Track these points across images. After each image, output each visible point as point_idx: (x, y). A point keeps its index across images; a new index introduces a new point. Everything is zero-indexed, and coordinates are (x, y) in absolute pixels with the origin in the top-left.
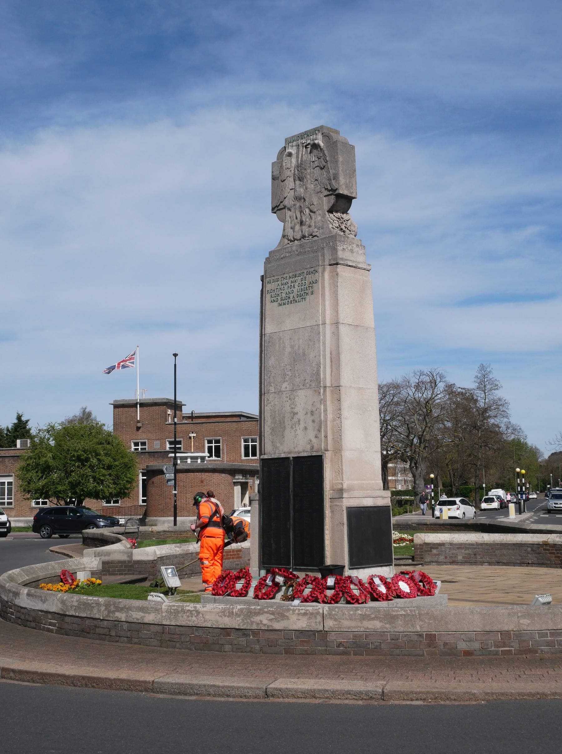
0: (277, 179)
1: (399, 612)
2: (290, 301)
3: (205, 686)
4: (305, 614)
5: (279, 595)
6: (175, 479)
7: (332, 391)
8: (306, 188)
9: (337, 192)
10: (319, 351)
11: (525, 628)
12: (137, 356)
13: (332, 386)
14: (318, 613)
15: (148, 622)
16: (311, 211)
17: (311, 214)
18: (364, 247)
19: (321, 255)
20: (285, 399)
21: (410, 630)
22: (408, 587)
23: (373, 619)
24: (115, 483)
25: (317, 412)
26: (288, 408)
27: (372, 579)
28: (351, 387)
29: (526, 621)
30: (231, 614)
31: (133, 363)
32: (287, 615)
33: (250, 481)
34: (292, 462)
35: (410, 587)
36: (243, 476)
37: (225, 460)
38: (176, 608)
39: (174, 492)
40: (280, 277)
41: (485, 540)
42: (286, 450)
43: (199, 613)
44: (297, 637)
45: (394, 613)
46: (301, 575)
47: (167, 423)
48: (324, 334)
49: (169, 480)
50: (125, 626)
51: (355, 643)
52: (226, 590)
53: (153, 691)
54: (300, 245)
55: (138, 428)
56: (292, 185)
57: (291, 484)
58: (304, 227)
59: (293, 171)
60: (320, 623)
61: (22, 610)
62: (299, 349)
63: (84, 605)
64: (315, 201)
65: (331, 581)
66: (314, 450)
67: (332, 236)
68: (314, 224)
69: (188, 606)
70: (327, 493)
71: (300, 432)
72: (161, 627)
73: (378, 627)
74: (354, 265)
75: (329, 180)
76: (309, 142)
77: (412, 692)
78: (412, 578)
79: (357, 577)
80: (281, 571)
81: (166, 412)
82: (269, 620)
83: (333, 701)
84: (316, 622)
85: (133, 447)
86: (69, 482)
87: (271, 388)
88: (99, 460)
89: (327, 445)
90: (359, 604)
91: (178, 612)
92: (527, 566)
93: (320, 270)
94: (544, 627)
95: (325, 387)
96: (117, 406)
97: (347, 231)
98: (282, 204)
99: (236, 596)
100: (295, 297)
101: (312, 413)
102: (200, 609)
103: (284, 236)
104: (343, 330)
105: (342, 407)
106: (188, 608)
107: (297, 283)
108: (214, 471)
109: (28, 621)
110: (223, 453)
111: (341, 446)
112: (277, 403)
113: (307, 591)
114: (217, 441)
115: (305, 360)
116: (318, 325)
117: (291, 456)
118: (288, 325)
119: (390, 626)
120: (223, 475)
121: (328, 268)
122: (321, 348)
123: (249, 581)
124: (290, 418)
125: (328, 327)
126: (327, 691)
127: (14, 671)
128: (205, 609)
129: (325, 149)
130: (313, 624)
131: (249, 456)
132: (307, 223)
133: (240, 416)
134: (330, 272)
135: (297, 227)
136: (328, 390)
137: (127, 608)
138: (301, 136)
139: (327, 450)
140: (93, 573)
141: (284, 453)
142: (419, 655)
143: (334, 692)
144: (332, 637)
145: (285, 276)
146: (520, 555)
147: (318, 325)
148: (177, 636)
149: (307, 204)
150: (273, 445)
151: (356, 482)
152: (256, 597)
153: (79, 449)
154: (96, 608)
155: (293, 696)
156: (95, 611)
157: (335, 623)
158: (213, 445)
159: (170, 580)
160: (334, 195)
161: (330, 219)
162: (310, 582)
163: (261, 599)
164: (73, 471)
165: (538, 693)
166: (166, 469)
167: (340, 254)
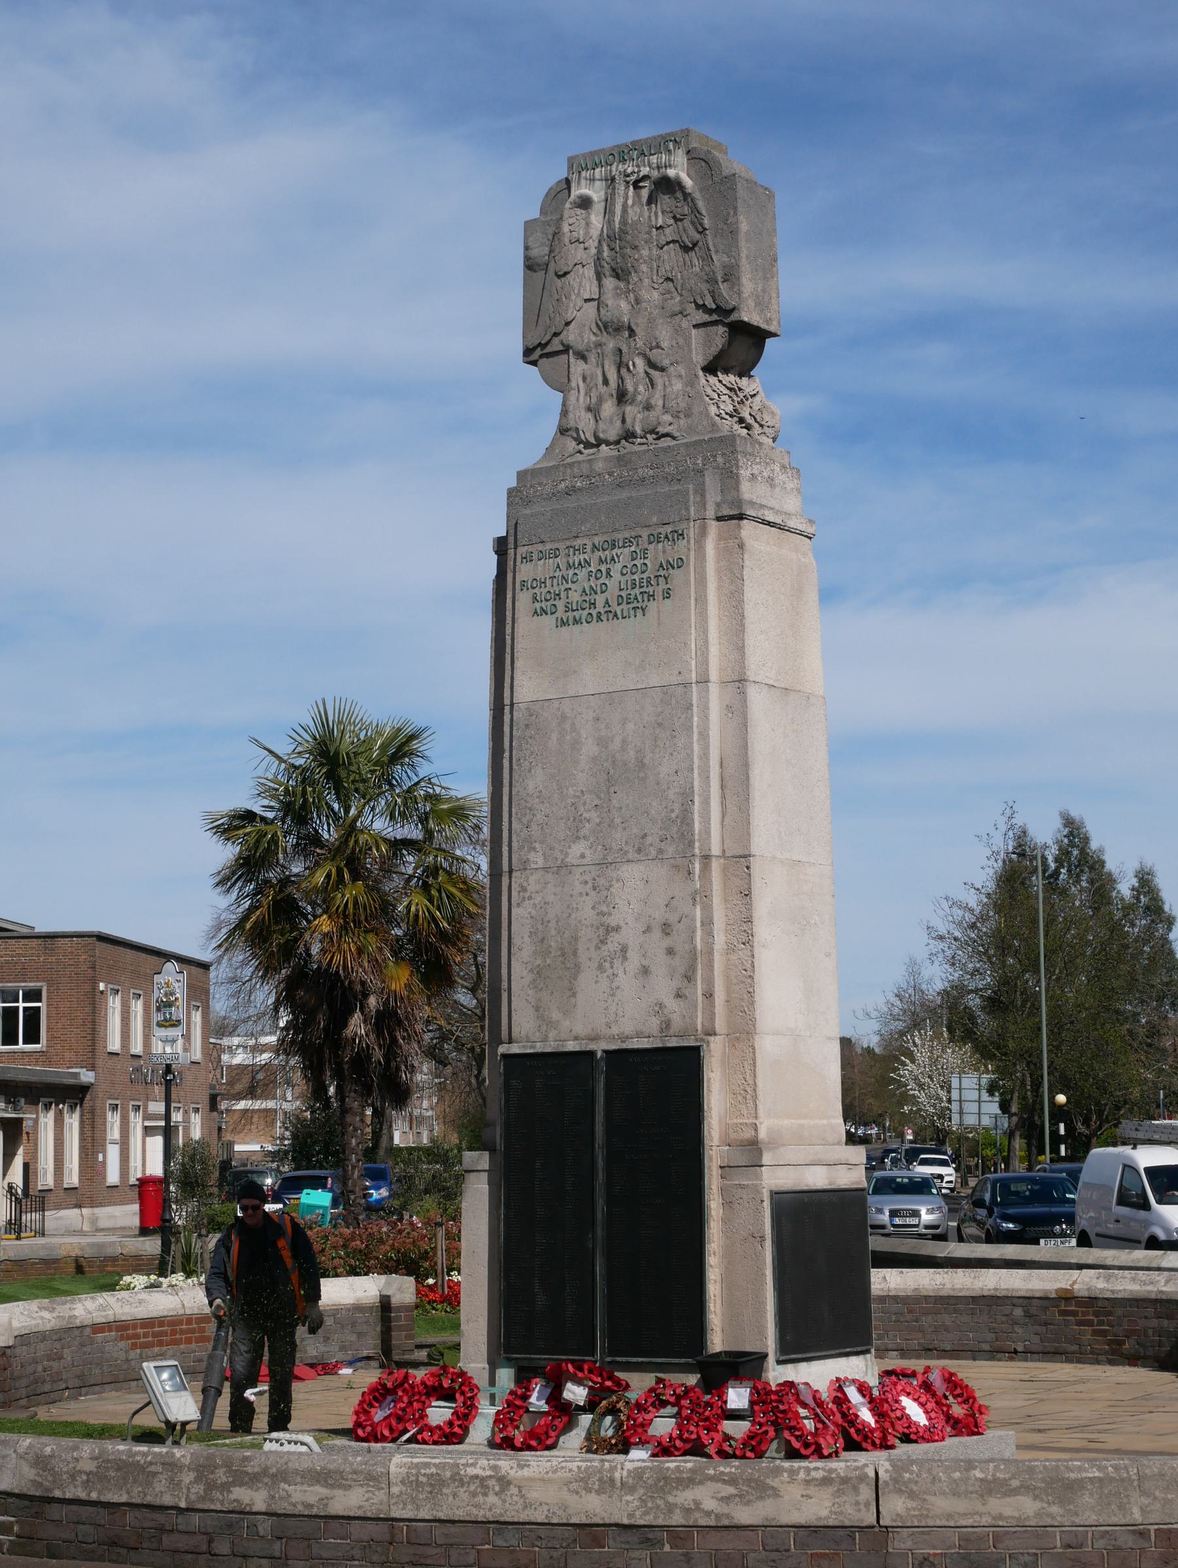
1: (1086, 1471)
2: (594, 613)
4: (826, 1481)
5: (574, 1440)
7: (725, 870)
8: (638, 301)
10: (690, 756)
13: (724, 854)
14: (863, 1478)
15: (341, 1513)
16: (651, 364)
17: (655, 374)
18: (798, 471)
19: (696, 492)
20: (579, 888)
21: (1114, 1520)
22: (920, 1411)
23: (1014, 1492)
25: (681, 926)
26: (587, 914)
27: (840, 1389)
28: (774, 858)
30: (607, 1485)
32: (774, 1484)
33: (28, 1116)
34: (603, 1064)
35: (926, 1412)
36: (8, 1102)
38: (433, 1470)
40: (562, 546)
41: (892, 1286)
42: (580, 1029)
43: (509, 1483)
45: (1073, 1476)
46: (639, 1384)
48: (705, 709)
50: (265, 1526)
51: (965, 1557)
52: (401, 1427)
54: (619, 459)
56: (589, 288)
57: (599, 1129)
58: (628, 409)
59: (593, 251)
60: (867, 1505)
62: (624, 749)
63: (119, 1469)
64: (665, 336)
65: (739, 1395)
66: (671, 1032)
67: (722, 439)
68: (660, 403)
69: (474, 1465)
70: (713, 1153)
71: (627, 980)
72: (385, 1527)
73: (1030, 1513)
74: (779, 521)
75: (712, 281)
76: (645, 171)
78: (927, 1386)
79: (807, 1384)
80: (581, 1369)
82: (722, 1499)
84: (857, 1503)
87: (532, 856)
90: (822, 1457)
91: (443, 1483)
92: (1011, 1359)
93: (692, 531)
97: (757, 429)
98: (556, 340)
99: (435, 1443)
100: (613, 603)
101: (666, 929)
102: (512, 1472)
103: (563, 431)
104: (757, 698)
105: (756, 915)
106: (471, 1471)
107: (618, 566)
111: (753, 1020)
112: (551, 898)
113: (663, 1425)
115: (643, 779)
116: (686, 685)
117: (599, 1047)
118: (589, 680)
119: (1061, 1511)
121: (713, 527)
122: (696, 747)
123: (473, 1398)
124: (595, 941)
125: (714, 690)
128: (526, 1472)
130: (849, 1509)
131: (17, 1043)
132: (639, 398)
134: (720, 538)
135: (609, 408)
136: (715, 865)
137: (274, 1476)
138: (622, 154)
139: (714, 1033)
141: (576, 1038)
144: (901, 1543)
145: (578, 543)
146: (991, 1330)
147: (686, 685)
148: (435, 1551)
149: (640, 344)
150: (541, 1017)
151: (786, 1122)
152: (502, 1443)
154: (162, 1477)
156: (160, 1484)
159: (170, 1401)
160: (725, 325)
161: (709, 391)
162: (672, 1399)
163: (521, 1450)
167: (747, 491)
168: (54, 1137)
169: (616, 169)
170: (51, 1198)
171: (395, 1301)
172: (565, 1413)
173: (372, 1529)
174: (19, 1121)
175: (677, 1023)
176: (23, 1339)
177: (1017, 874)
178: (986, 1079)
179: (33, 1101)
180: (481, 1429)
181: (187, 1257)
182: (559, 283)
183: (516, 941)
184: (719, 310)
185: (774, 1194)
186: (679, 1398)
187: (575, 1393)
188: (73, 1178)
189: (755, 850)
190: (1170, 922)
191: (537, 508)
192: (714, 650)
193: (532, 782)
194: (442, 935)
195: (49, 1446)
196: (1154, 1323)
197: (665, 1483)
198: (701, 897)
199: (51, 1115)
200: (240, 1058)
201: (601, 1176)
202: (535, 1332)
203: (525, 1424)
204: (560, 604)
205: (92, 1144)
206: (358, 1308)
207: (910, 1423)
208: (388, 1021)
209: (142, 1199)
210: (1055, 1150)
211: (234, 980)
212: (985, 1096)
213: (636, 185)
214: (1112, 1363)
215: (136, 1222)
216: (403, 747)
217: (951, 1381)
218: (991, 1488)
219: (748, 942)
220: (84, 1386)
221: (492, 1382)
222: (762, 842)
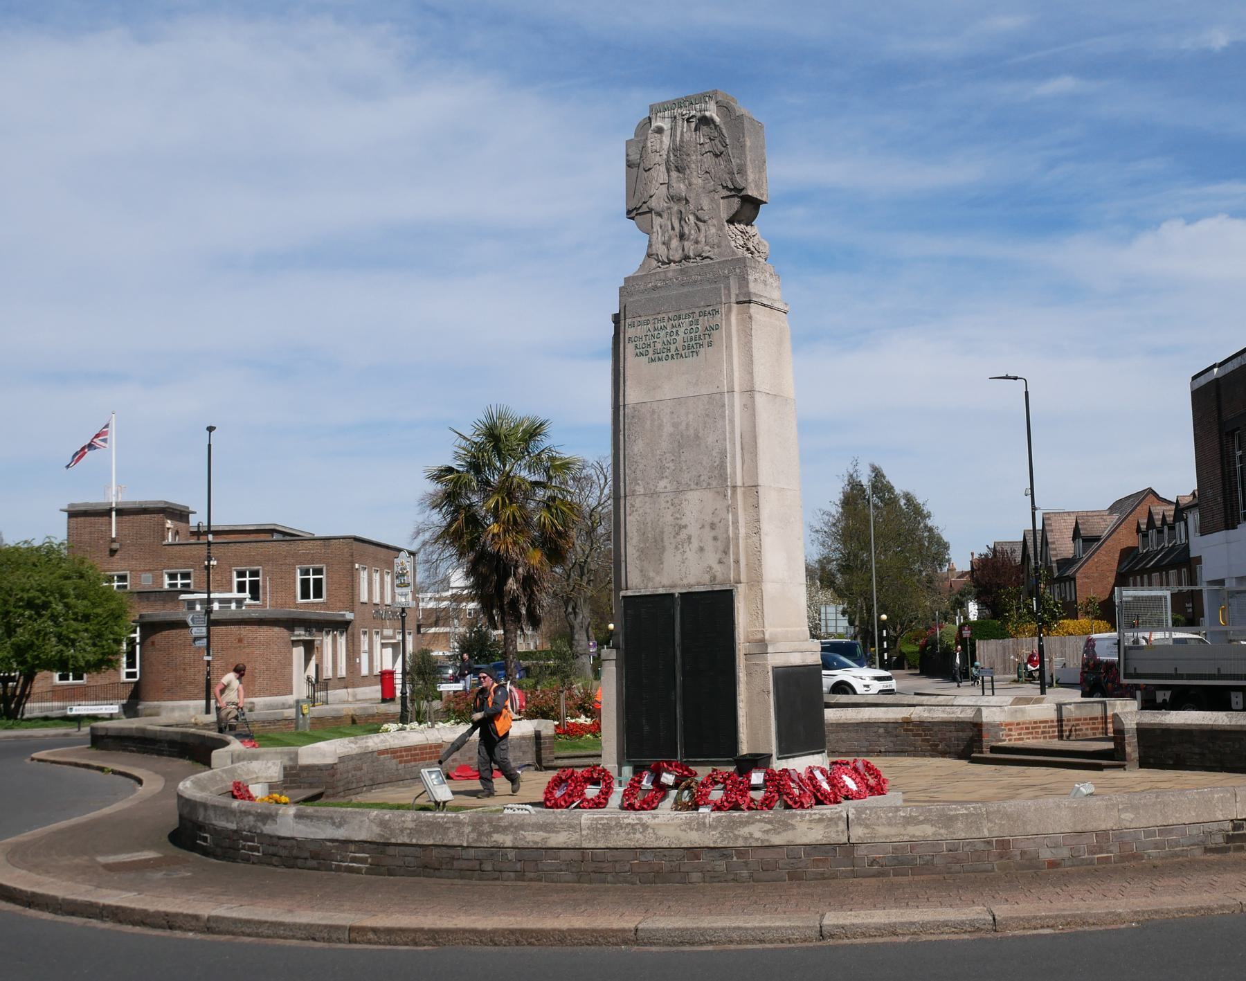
3: (723, 929)
4: (820, 820)
5: (669, 802)
6: (208, 637)
7: (744, 493)
8: (690, 184)
9: (743, 193)
10: (724, 432)
11: (1128, 825)
12: (113, 430)
14: (840, 818)
16: (698, 219)
17: (700, 224)
20: (664, 505)
23: (922, 822)
24: (94, 645)
26: (668, 518)
27: (811, 772)
29: (1127, 816)
30: (702, 826)
31: (105, 441)
33: (317, 638)
37: (267, 605)
39: (206, 658)
40: (651, 318)
42: (666, 582)
44: (807, 854)
46: (702, 772)
47: (165, 542)
48: (732, 406)
49: (196, 639)
50: (512, 855)
51: (894, 858)
53: (636, 942)
55: (113, 552)
56: (663, 177)
58: (686, 243)
61: (282, 842)
62: (687, 429)
64: (705, 203)
67: (738, 259)
71: (691, 554)
76: (693, 113)
77: (1035, 918)
78: (856, 769)
81: (163, 525)
83: (924, 938)
85: (167, 581)
86: (12, 644)
87: (637, 488)
88: (67, 606)
89: (739, 575)
91: (611, 828)
93: (723, 310)
94: (1152, 823)
95: (734, 487)
96: (74, 514)
101: (713, 526)
103: (649, 255)
104: (760, 400)
106: (627, 821)
108: (260, 622)
109: (297, 858)
110: (265, 593)
114: (254, 574)
116: (722, 393)
118: (668, 391)
120: (276, 629)
125: (737, 396)
126: (913, 923)
127: (375, 930)
128: (657, 821)
129: (722, 126)
133: (272, 531)
135: (675, 243)
136: (739, 491)
140: (272, 787)
142: (987, 871)
143: (923, 925)
144: (860, 852)
145: (659, 317)
147: (722, 393)
150: (644, 576)
151: (779, 630)
153: (32, 587)
155: (864, 935)
157: (866, 831)
158: (247, 579)
164: (19, 626)
165: (1202, 908)
166: (193, 620)
167: (753, 288)
168: (332, 648)
169: (677, 112)
170: (331, 683)
171: (543, 733)
172: (662, 789)
173: (572, 854)
175: (720, 577)
177: (853, 499)
178: (840, 608)
180: (615, 799)
181: (418, 713)
182: (646, 174)
183: (629, 534)
184: (735, 189)
185: (774, 668)
186: (725, 779)
187: (668, 779)
188: (342, 672)
189: (760, 483)
191: (636, 298)
192: (736, 374)
193: (636, 447)
194: (559, 534)
195: (388, 815)
196: (955, 734)
197: (733, 825)
198: (732, 508)
199: (330, 637)
200: (431, 605)
201: (679, 660)
202: (643, 746)
204: (651, 350)
206: (523, 738)
207: (848, 789)
208: (529, 582)
209: (383, 683)
210: (881, 645)
211: (427, 562)
212: (840, 616)
213: (688, 121)
214: (932, 756)
215: (379, 695)
216: (534, 432)
217: (868, 767)
218: (908, 821)
219: (758, 533)
220: (374, 784)
221: (620, 774)
222: (762, 480)
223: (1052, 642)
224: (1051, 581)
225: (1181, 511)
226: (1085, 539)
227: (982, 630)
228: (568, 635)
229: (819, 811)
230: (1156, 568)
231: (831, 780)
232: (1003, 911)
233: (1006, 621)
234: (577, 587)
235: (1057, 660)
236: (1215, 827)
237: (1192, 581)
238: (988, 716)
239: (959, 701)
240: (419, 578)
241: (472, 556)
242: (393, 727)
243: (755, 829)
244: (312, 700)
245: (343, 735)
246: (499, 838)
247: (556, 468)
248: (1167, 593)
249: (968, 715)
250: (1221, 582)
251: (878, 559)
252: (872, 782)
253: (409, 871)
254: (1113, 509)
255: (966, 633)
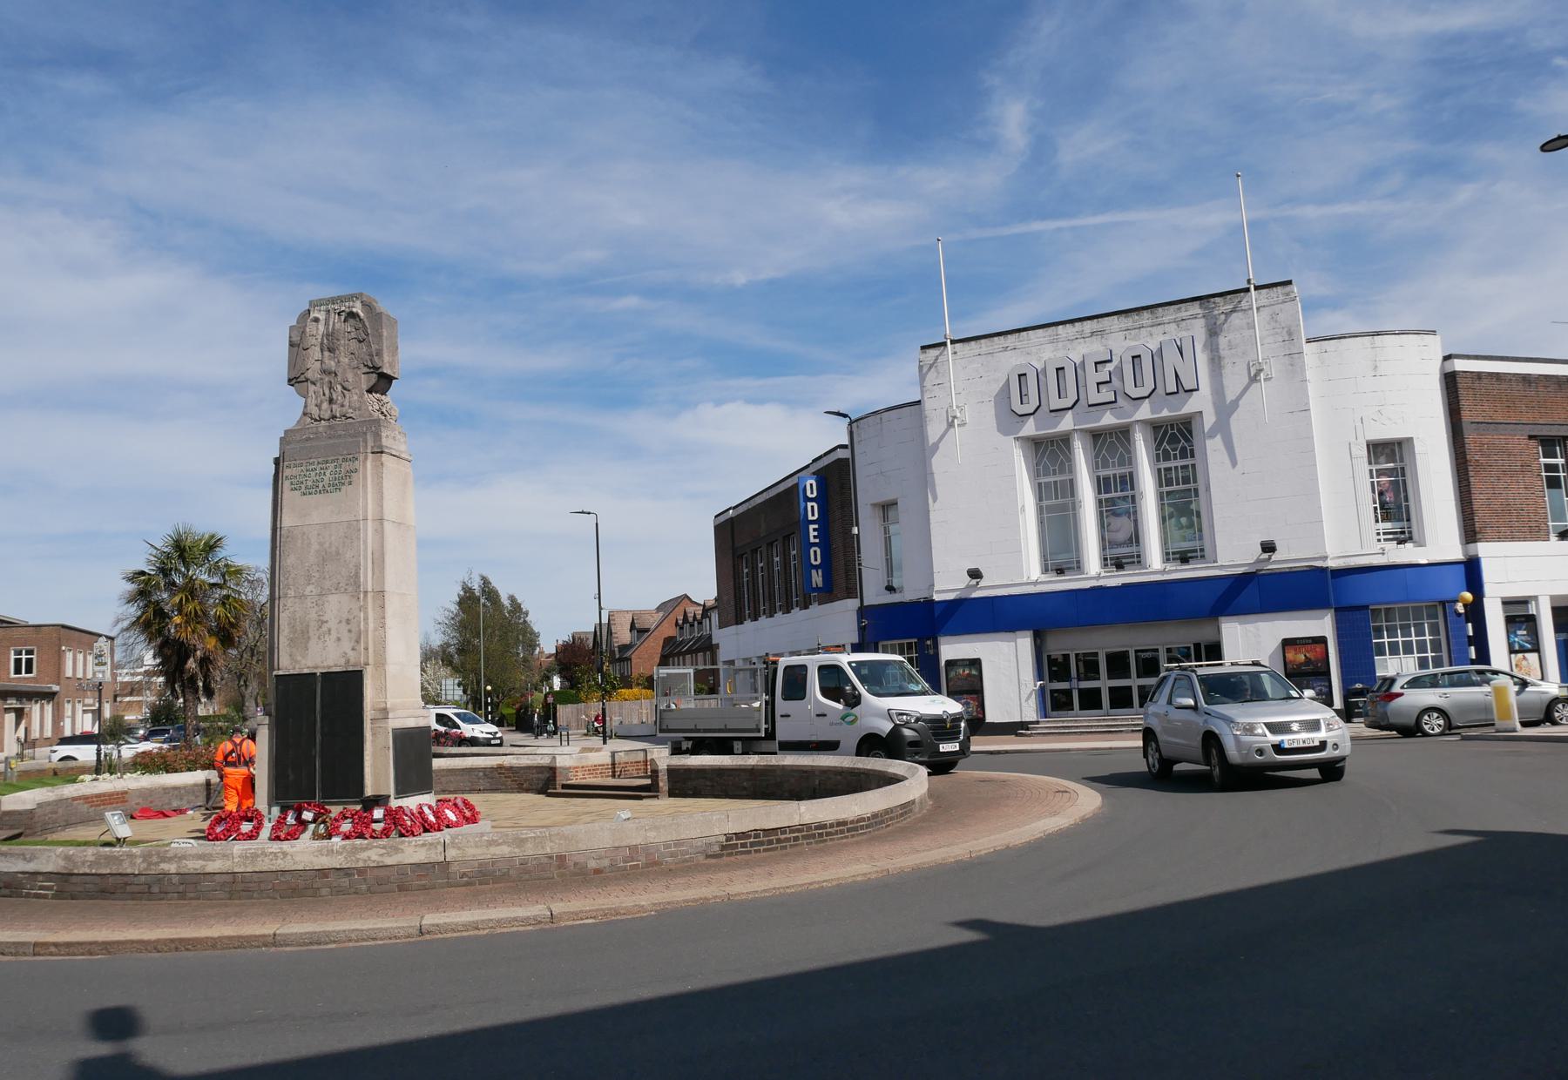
0: (297, 346)
26: (313, 615)
29: (652, 834)
30: (330, 852)
33: (27, 706)
46: (335, 810)
50: (175, 879)
53: (274, 944)
56: (318, 355)
83: (499, 930)
93: (361, 458)
101: (348, 622)
103: (305, 414)
104: (387, 526)
117: (318, 671)
118: (316, 518)
125: (370, 523)
127: (56, 945)
135: (325, 405)
136: (370, 595)
138: (333, 301)
143: (499, 921)
144: (454, 868)
155: (453, 930)
158: (24, 657)
167: (385, 442)
168: (40, 716)
169: (330, 307)
172: (303, 824)
174: (22, 709)
175: (352, 661)
176: (40, 805)
177: (468, 600)
179: (30, 700)
180: (265, 832)
188: (48, 733)
190: (527, 614)
192: (370, 506)
193: (289, 561)
195: (71, 851)
197: (355, 850)
198: (363, 608)
200: (127, 679)
202: (289, 791)
203: (285, 830)
205: (58, 718)
206: (196, 785)
208: (205, 662)
216: (212, 545)
217: (466, 803)
218: (491, 843)
219: (383, 627)
220: (68, 825)
222: (389, 586)
223: (613, 706)
224: (613, 661)
225: (706, 611)
226: (639, 630)
227: (562, 697)
228: (239, 706)
229: (428, 837)
230: (689, 651)
231: (436, 814)
232: (558, 907)
233: (579, 690)
234: (248, 666)
235: (616, 719)
236: (713, 839)
237: (714, 662)
238: (561, 762)
239: (540, 751)
240: (116, 658)
241: (159, 640)
242: (88, 777)
243: (373, 853)
244: (20, 756)
245: (44, 785)
246: (165, 867)
247: (230, 573)
248: (691, 671)
249: (546, 761)
250: (732, 662)
251: (486, 649)
252: (468, 814)
253: (89, 896)
254: (659, 609)
255: (550, 700)
